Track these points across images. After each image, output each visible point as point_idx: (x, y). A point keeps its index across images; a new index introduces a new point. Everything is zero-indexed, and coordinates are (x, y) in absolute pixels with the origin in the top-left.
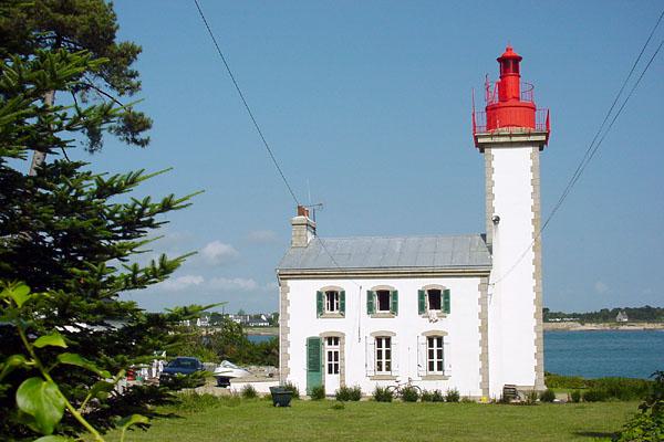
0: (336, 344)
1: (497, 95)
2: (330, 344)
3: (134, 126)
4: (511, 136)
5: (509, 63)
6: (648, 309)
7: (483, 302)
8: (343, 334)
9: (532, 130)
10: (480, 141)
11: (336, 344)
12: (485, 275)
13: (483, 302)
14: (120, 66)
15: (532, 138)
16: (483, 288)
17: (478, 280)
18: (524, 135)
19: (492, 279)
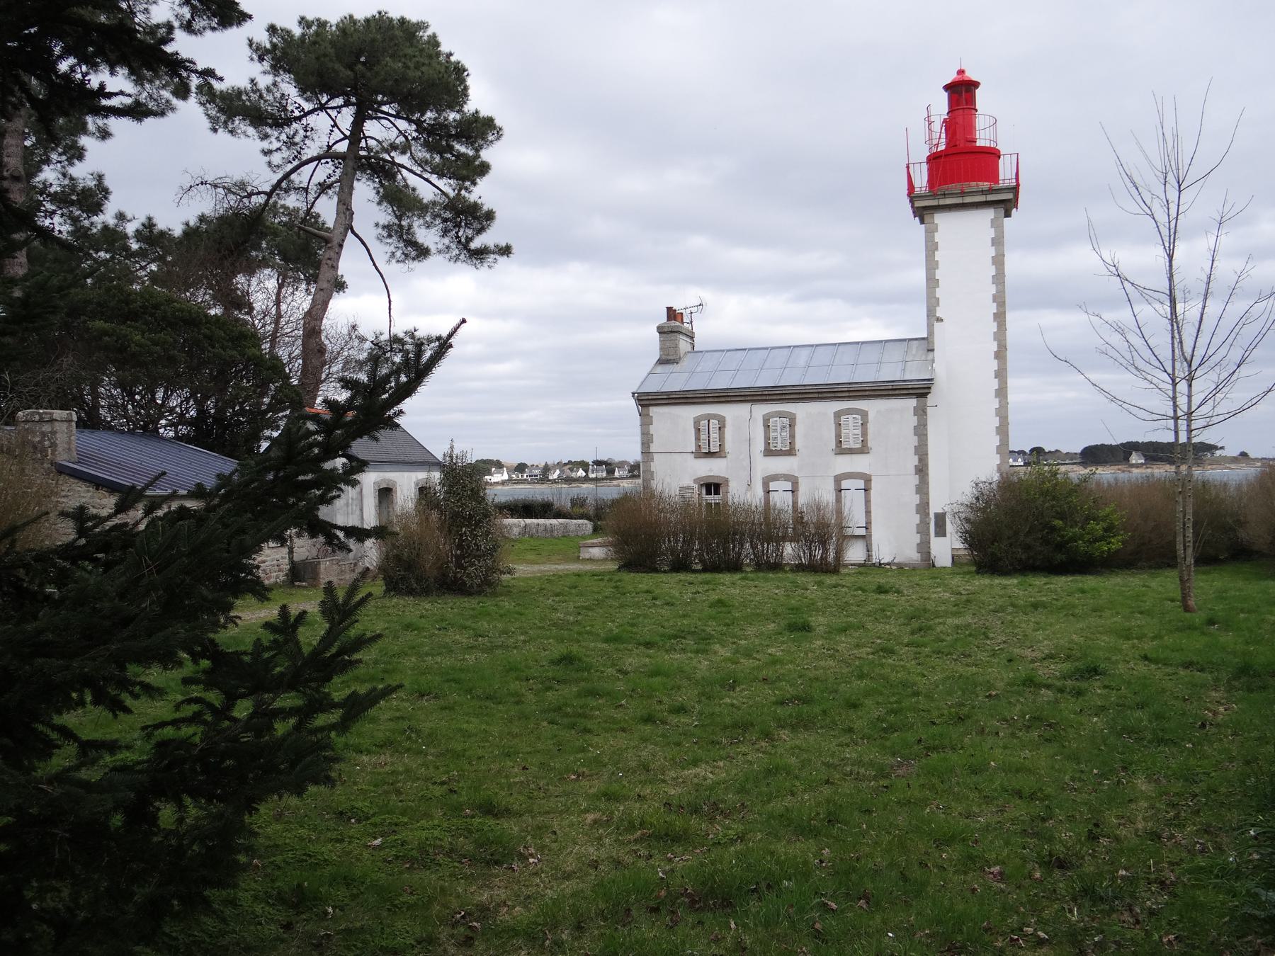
0: (717, 492)
1: (943, 136)
2: (708, 493)
3: (267, 153)
4: (963, 194)
5: (464, 321)
6: (995, 298)
7: (921, 431)
8: (727, 481)
9: (995, 186)
10: (917, 204)
11: (717, 492)
12: (920, 391)
13: (921, 431)
14: (465, 70)
15: (991, 198)
16: (921, 412)
17: (912, 402)
18: (983, 192)
19: (930, 399)
